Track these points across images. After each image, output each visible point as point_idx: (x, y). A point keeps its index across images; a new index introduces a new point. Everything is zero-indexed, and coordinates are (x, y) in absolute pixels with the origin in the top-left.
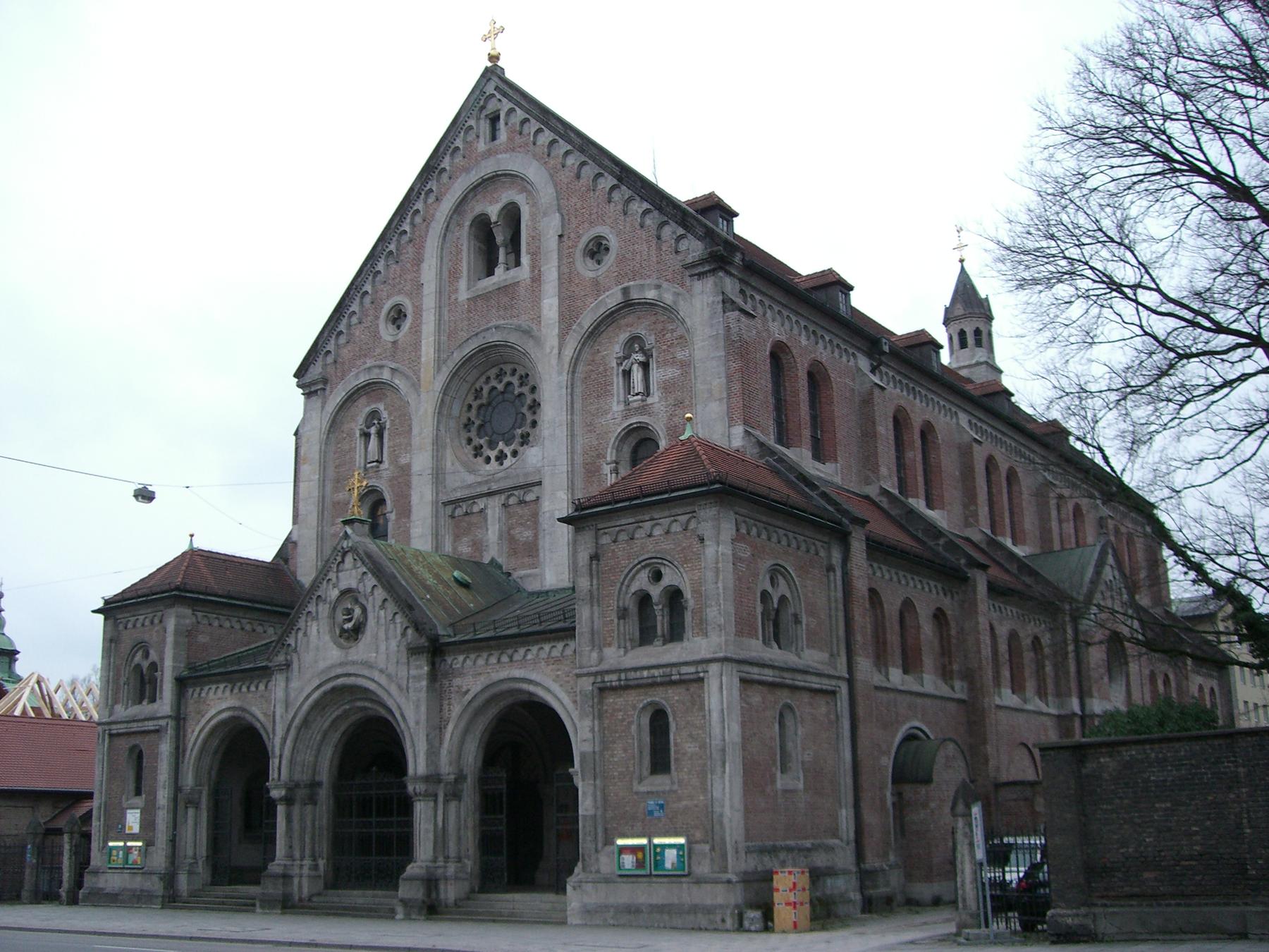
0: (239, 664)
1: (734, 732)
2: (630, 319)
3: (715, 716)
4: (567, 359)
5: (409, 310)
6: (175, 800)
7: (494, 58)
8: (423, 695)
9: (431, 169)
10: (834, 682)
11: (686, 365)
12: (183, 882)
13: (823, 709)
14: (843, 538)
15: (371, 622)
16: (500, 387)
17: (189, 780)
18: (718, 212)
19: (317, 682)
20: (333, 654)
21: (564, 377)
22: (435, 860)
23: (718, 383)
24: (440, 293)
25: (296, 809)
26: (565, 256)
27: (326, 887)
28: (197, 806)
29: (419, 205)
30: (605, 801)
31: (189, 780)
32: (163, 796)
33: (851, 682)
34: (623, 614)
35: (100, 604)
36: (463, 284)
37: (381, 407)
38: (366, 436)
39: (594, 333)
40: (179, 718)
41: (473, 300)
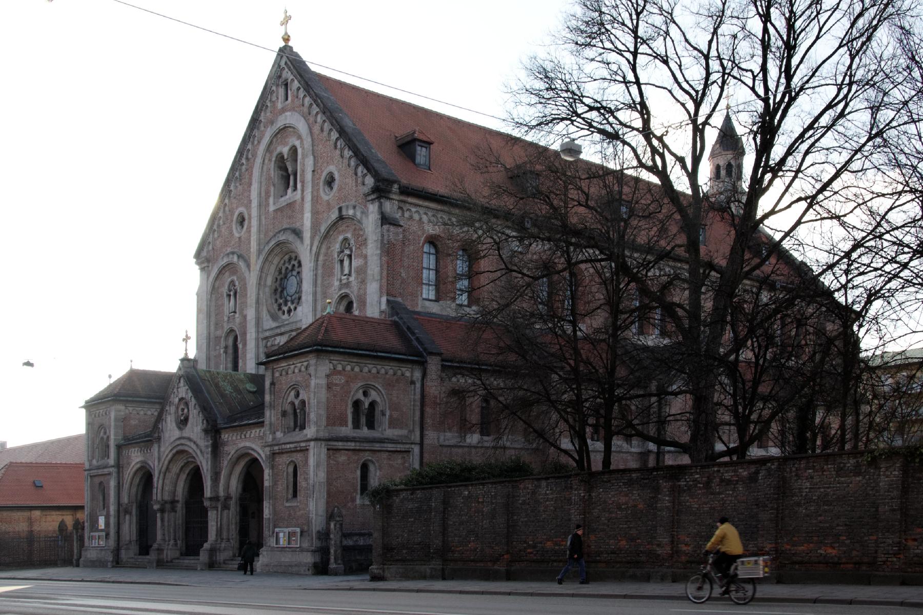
0: (242, 421)
1: (322, 475)
2: (343, 227)
3: (312, 469)
4: (314, 252)
5: (246, 217)
6: (119, 511)
7: (286, 39)
8: (209, 456)
9: (255, 122)
10: (407, 446)
11: (366, 257)
12: (123, 555)
13: (400, 461)
14: (422, 364)
15: (191, 417)
16: (290, 267)
17: (125, 500)
18: (417, 143)
19: (170, 448)
20: (177, 433)
21: (312, 264)
22: (216, 541)
23: (377, 270)
24: (260, 205)
25: (166, 515)
26: (315, 185)
27: (181, 554)
28: (130, 514)
29: (249, 146)
30: (275, 512)
31: (125, 500)
32: (112, 509)
33: (421, 444)
34: (284, 414)
35: (83, 404)
36: (271, 200)
37: (235, 278)
38: (229, 296)
39: (326, 236)
40: (119, 466)
41: (276, 211)
